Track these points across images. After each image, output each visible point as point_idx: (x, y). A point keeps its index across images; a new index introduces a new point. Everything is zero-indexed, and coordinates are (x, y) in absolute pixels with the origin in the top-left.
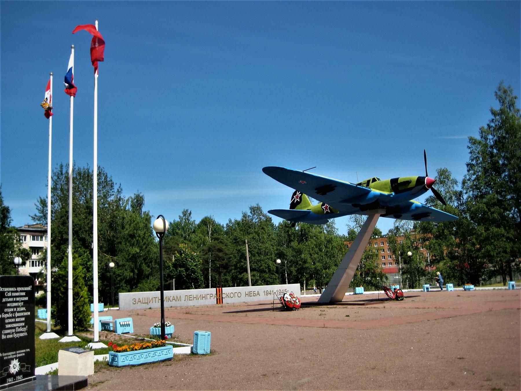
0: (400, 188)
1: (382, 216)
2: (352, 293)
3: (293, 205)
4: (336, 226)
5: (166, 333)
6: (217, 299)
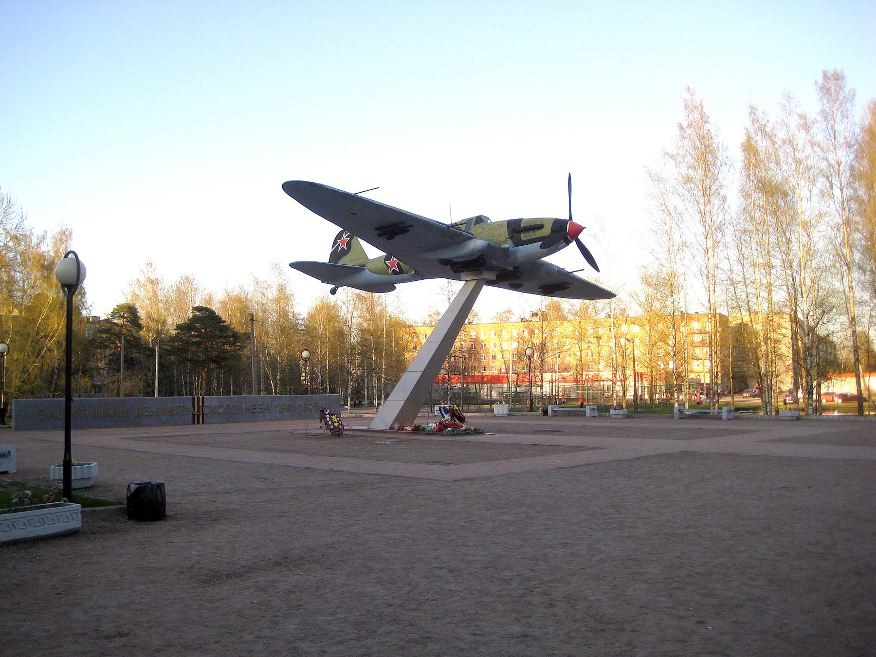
0: (524, 237)
1: (490, 283)
2: (315, 426)
3: (336, 255)
4: (848, 379)
5: (73, 477)
6: (194, 416)
